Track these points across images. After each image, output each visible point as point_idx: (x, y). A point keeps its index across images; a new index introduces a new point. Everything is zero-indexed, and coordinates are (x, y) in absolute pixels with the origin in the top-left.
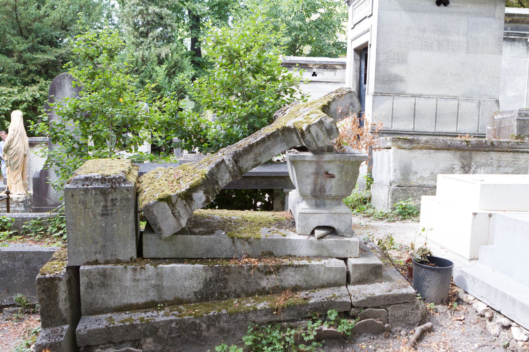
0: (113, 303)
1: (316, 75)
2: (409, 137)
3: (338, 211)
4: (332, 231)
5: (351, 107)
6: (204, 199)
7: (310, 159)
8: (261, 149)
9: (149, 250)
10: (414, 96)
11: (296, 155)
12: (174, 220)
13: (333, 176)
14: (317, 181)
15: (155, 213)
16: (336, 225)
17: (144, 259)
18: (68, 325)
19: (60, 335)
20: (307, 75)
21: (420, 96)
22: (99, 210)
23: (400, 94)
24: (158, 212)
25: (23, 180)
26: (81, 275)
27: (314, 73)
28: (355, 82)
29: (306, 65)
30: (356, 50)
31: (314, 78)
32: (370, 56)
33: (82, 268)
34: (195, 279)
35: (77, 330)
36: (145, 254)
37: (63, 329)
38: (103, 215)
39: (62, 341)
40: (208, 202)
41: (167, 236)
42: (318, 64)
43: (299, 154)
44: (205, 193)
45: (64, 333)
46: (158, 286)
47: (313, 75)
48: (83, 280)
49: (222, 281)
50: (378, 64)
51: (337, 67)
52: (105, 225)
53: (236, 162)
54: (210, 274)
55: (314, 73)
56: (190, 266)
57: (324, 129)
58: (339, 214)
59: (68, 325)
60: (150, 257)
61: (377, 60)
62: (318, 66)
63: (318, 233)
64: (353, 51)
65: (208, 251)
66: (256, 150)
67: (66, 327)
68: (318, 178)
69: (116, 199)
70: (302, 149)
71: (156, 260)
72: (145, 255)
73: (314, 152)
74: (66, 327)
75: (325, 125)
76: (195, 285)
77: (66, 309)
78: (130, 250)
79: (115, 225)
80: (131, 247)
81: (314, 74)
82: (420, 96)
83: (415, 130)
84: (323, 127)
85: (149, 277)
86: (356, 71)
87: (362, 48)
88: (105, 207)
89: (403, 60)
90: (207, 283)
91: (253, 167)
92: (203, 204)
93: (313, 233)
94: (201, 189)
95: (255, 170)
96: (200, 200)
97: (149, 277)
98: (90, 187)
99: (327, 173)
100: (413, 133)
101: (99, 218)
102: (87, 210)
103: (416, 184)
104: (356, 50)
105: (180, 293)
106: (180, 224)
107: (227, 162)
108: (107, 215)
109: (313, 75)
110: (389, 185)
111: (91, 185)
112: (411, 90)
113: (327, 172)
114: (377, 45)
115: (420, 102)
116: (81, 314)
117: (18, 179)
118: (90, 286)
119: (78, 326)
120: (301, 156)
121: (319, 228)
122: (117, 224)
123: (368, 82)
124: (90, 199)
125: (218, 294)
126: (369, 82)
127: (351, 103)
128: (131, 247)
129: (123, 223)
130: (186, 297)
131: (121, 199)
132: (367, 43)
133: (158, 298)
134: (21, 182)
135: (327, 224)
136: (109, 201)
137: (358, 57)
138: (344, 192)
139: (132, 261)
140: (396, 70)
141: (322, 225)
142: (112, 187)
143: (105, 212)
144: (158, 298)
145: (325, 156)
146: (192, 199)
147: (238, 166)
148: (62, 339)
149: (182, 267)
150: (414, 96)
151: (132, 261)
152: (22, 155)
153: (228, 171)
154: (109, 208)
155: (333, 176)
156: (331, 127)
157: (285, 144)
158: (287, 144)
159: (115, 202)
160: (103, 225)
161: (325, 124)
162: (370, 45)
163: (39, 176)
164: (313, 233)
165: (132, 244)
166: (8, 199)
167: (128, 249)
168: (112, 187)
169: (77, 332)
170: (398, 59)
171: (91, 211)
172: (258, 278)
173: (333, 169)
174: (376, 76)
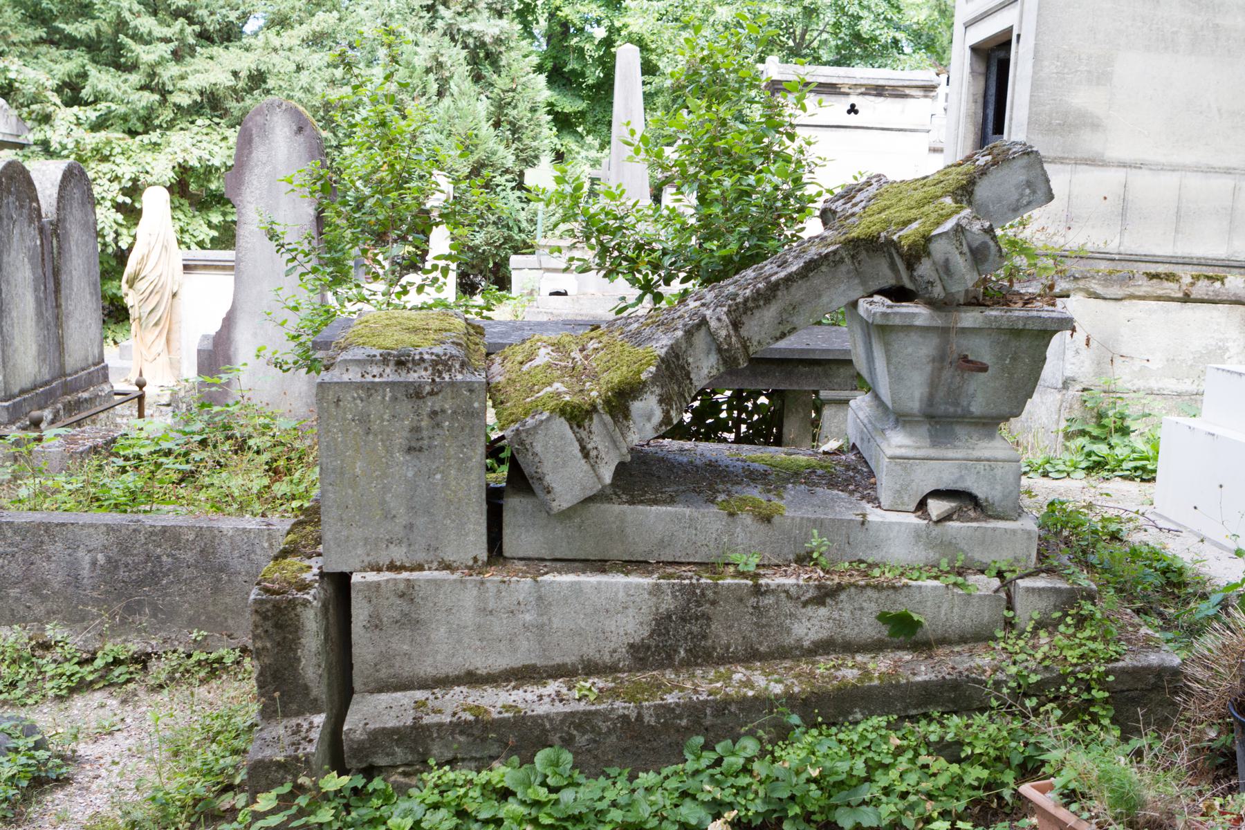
0: (427, 669)
1: (856, 112)
2: (1161, 269)
3: (987, 454)
4: (964, 500)
5: (1028, 191)
6: (658, 416)
7: (926, 323)
8: (798, 291)
9: (517, 540)
10: (1123, 165)
11: (889, 311)
12: (586, 467)
13: (983, 368)
14: (939, 377)
15: (538, 448)
16: (980, 491)
17: (505, 558)
18: (323, 716)
19: (304, 739)
20: (835, 110)
21: (1138, 166)
22: (400, 439)
23: (1094, 161)
24: (545, 446)
25: (169, 352)
26: (353, 595)
27: (853, 106)
28: (971, 128)
29: (833, 86)
30: (975, 49)
31: (852, 119)
32: (1016, 63)
33: (356, 578)
34: (631, 612)
35: (345, 728)
36: (508, 549)
37: (311, 723)
38: (410, 450)
39: (313, 754)
40: (666, 425)
41: (565, 506)
42: (861, 85)
43: (896, 310)
44: (660, 402)
45: (315, 735)
46: (541, 627)
47: (849, 112)
48: (360, 612)
49: (697, 619)
50: (1036, 85)
51: (907, 91)
52: (415, 475)
53: (736, 325)
54: (668, 603)
55: (853, 106)
56: (620, 579)
57: (965, 249)
58: (988, 460)
59: (323, 716)
60: (521, 555)
61: (1035, 73)
62: (863, 90)
63: (937, 507)
64: (968, 52)
65: (662, 544)
66: (783, 299)
67: (319, 719)
68: (941, 369)
69: (443, 411)
70: (898, 294)
71: (536, 563)
72: (507, 552)
73: (932, 303)
74: (319, 719)
75: (969, 238)
76: (630, 628)
77: (320, 676)
78: (472, 538)
79: (438, 476)
80: (475, 530)
81: (853, 110)
82: (1138, 166)
83: (1122, 249)
84: (964, 243)
85: (519, 603)
86: (975, 102)
87: (993, 44)
88: (416, 430)
89: (1100, 77)
90: (662, 624)
91: (777, 339)
92: (656, 430)
93: (922, 506)
94: (652, 393)
95: (782, 344)
96: (649, 420)
97: (519, 603)
98: (377, 380)
99: (965, 359)
100: (1117, 257)
101: (400, 457)
102: (371, 437)
103: (1129, 385)
104: (975, 49)
105: (593, 646)
106: (599, 478)
107: (713, 324)
108: (421, 450)
109: (849, 112)
110: (1060, 385)
111: (381, 375)
112: (1115, 152)
113: (966, 357)
114: (1037, 36)
115: (1141, 181)
116: (353, 688)
117: (159, 350)
118: (375, 624)
119: (348, 718)
120: (902, 314)
121: (937, 494)
122: (442, 472)
123: (1010, 128)
124: (377, 408)
125: (686, 651)
126: (1014, 128)
127: (1028, 181)
128: (475, 530)
129: (459, 470)
130: (607, 658)
131: (454, 412)
132: (1010, 30)
133: (539, 657)
134: (164, 358)
135: (960, 486)
136: (425, 417)
137: (981, 68)
138: (1005, 409)
139: (474, 568)
140: (1082, 99)
141: (942, 487)
142: (433, 380)
143: (413, 444)
144: (539, 657)
145: (963, 315)
146: (627, 416)
147: (738, 336)
148: (311, 749)
149: (599, 583)
150: (1123, 165)
151: (474, 568)
152: (168, 295)
153: (714, 348)
154: (425, 433)
155: (983, 368)
156: (985, 245)
157: (857, 281)
158: (864, 283)
159: (439, 418)
160: (410, 474)
161: (968, 234)
162: (1019, 36)
163: (210, 347)
164: (922, 506)
165: (479, 524)
166: (141, 398)
167: (467, 534)
168: (433, 380)
169: (347, 734)
170: (1089, 72)
171: (382, 440)
172: (786, 616)
173: (982, 350)
174: (1030, 113)
